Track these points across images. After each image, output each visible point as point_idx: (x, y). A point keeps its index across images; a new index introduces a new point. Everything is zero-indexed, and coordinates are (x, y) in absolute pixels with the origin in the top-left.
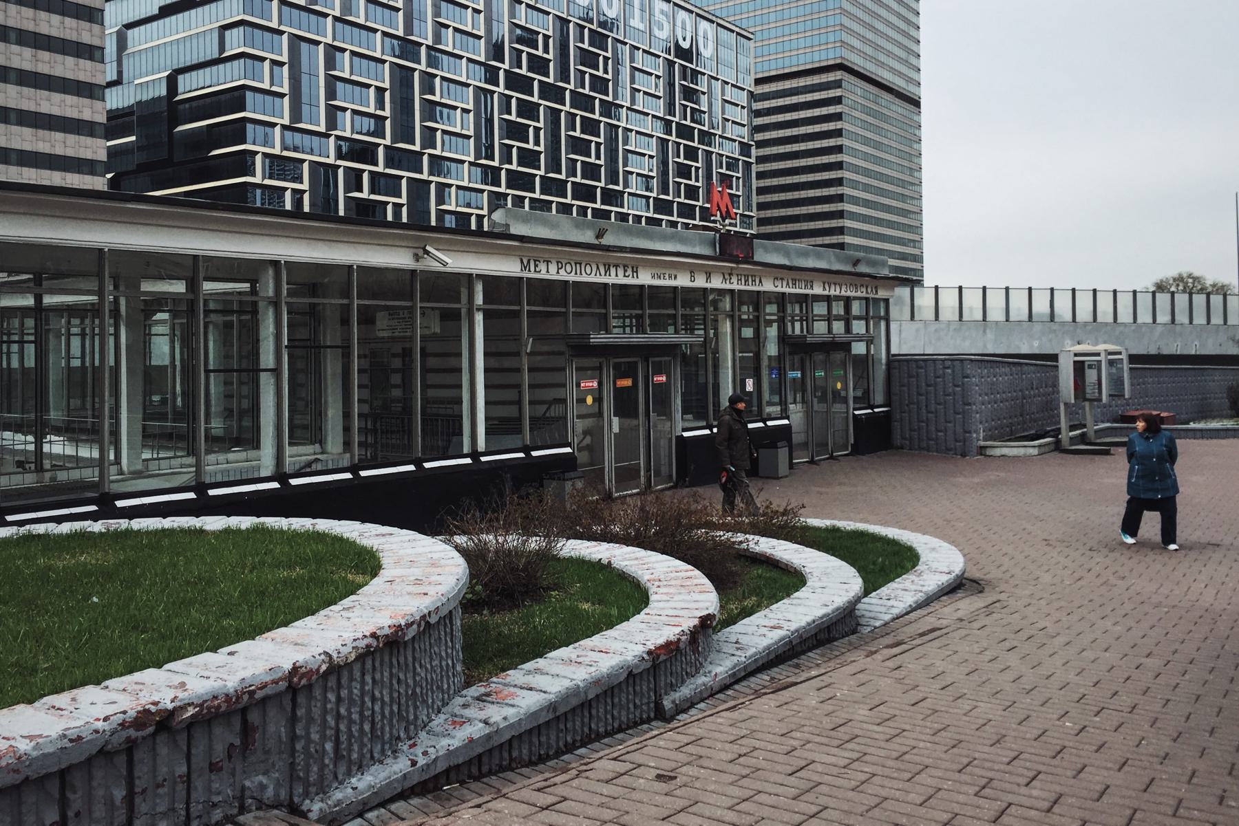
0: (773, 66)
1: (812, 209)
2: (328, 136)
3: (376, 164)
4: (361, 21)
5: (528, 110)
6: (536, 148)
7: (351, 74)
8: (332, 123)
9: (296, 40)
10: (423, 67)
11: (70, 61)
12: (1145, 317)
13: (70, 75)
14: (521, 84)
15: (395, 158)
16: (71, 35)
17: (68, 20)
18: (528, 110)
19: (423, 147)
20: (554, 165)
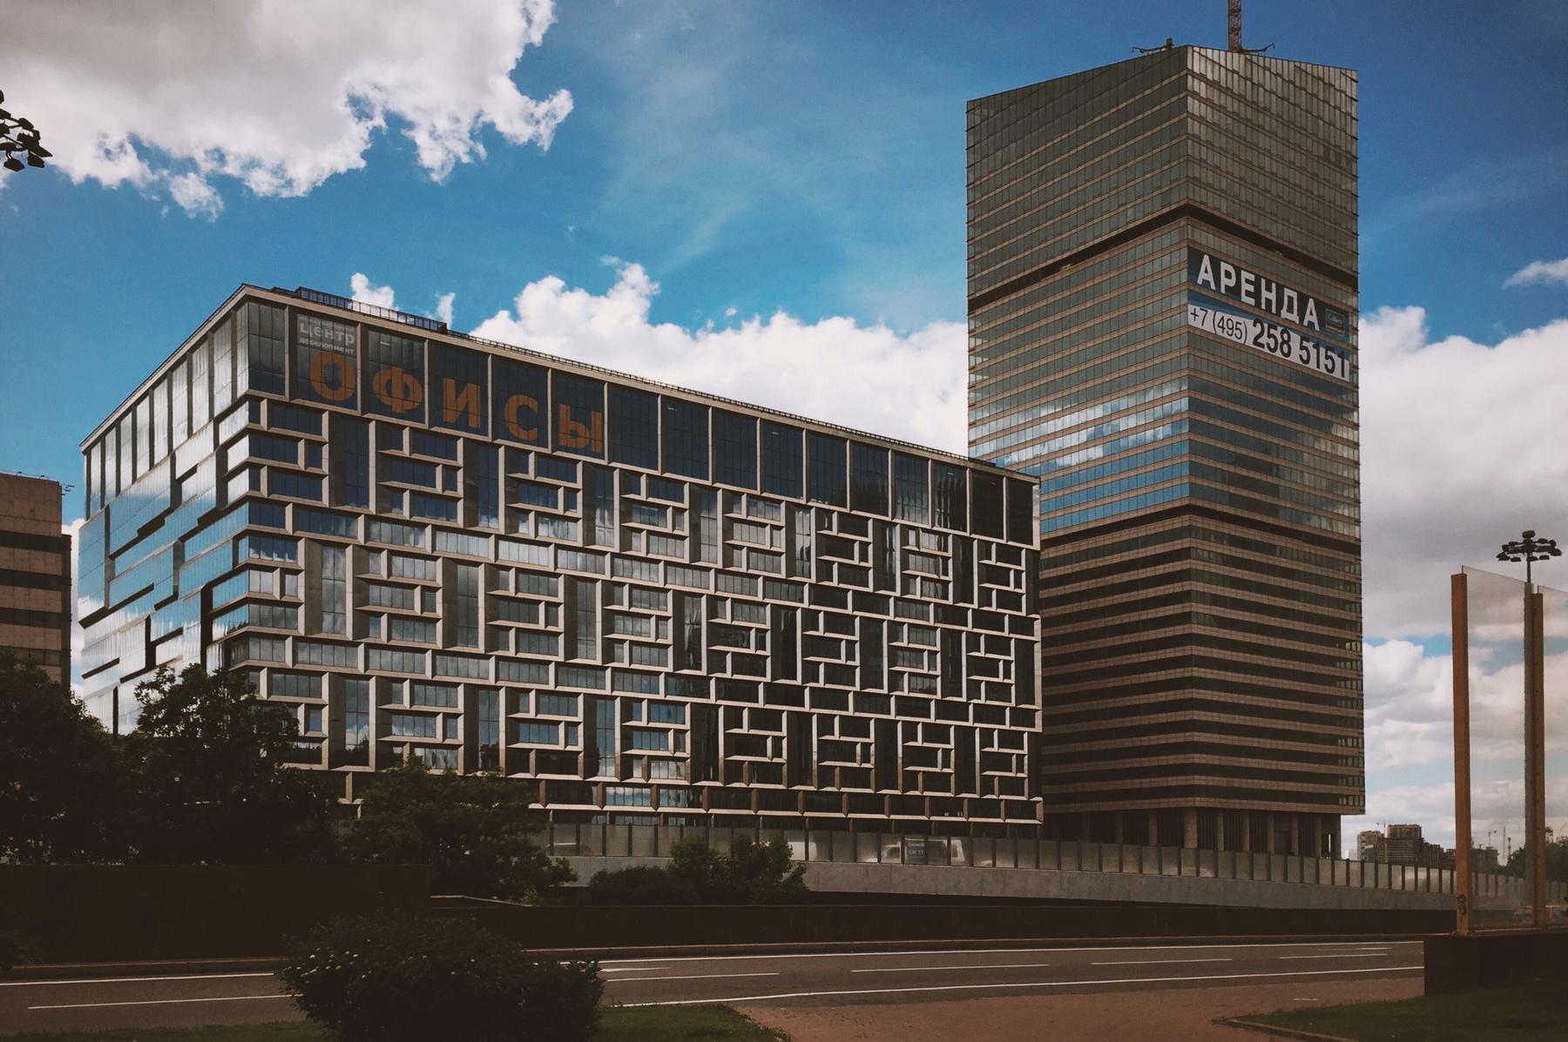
0: (1060, 524)
1: (1162, 696)
2: (355, 645)
3: (757, 701)
4: (743, 569)
5: (840, 623)
6: (760, 652)
7: (517, 591)
8: (609, 655)
9: (679, 596)
10: (891, 617)
11: (20, 591)
12: (1355, 883)
13: (20, 606)
14: (995, 621)
15: (945, 710)
16: (23, 567)
17: (18, 552)
18: (834, 622)
19: (890, 690)
20: (872, 677)
